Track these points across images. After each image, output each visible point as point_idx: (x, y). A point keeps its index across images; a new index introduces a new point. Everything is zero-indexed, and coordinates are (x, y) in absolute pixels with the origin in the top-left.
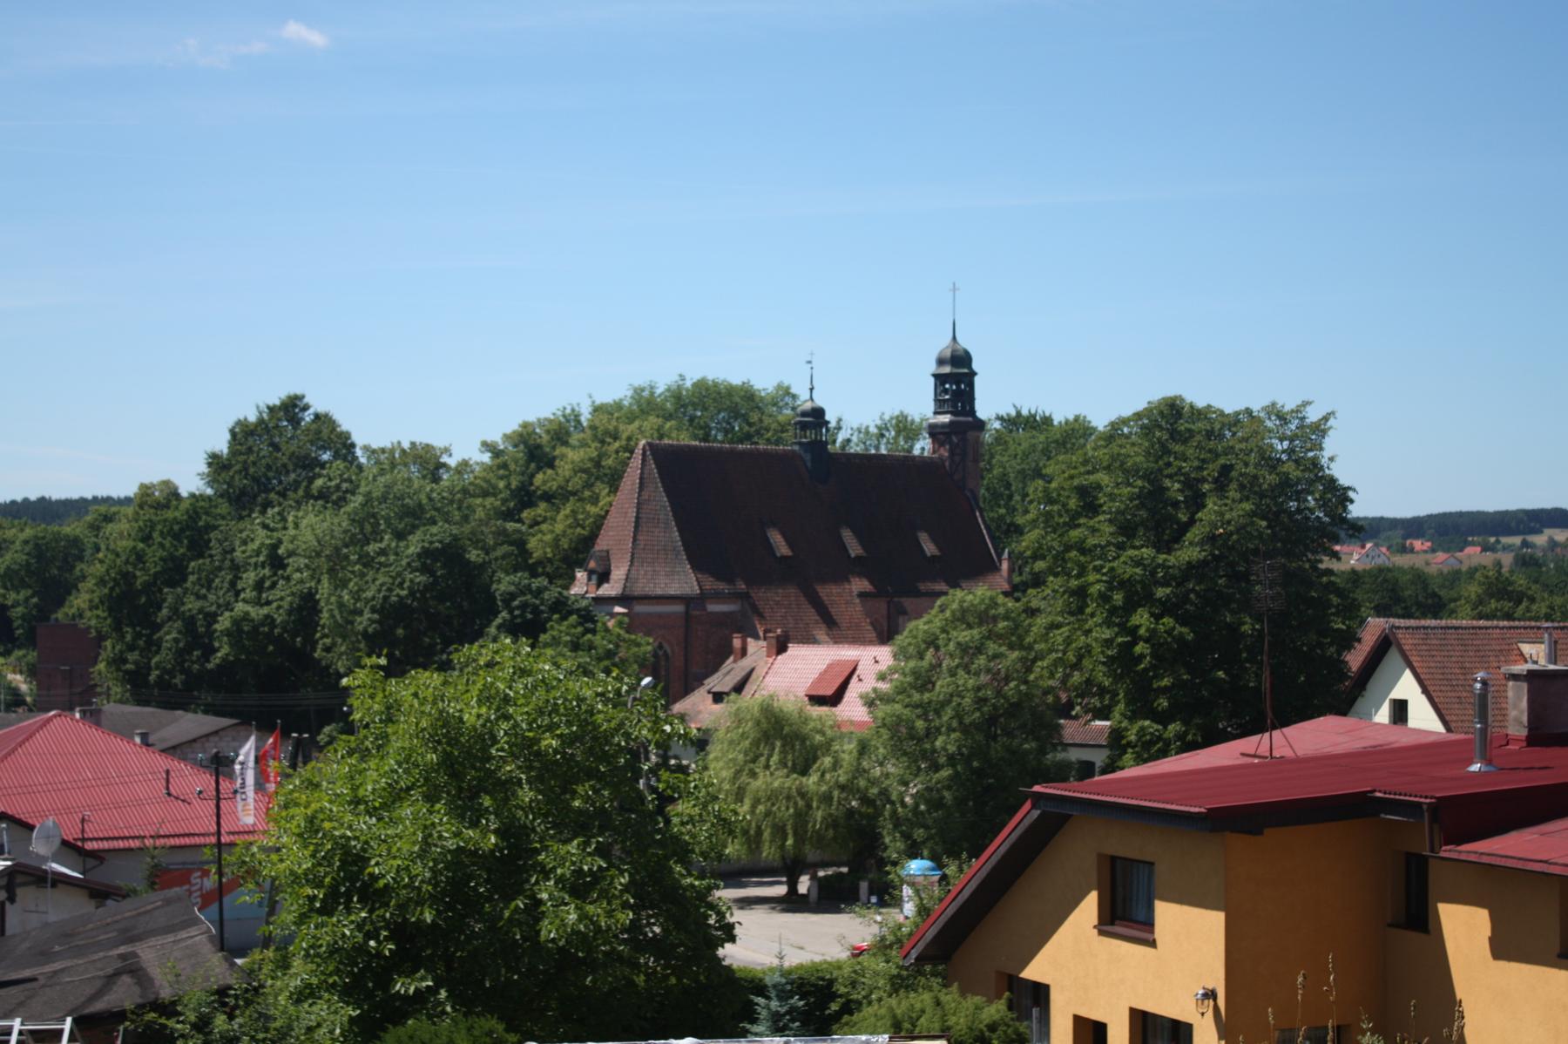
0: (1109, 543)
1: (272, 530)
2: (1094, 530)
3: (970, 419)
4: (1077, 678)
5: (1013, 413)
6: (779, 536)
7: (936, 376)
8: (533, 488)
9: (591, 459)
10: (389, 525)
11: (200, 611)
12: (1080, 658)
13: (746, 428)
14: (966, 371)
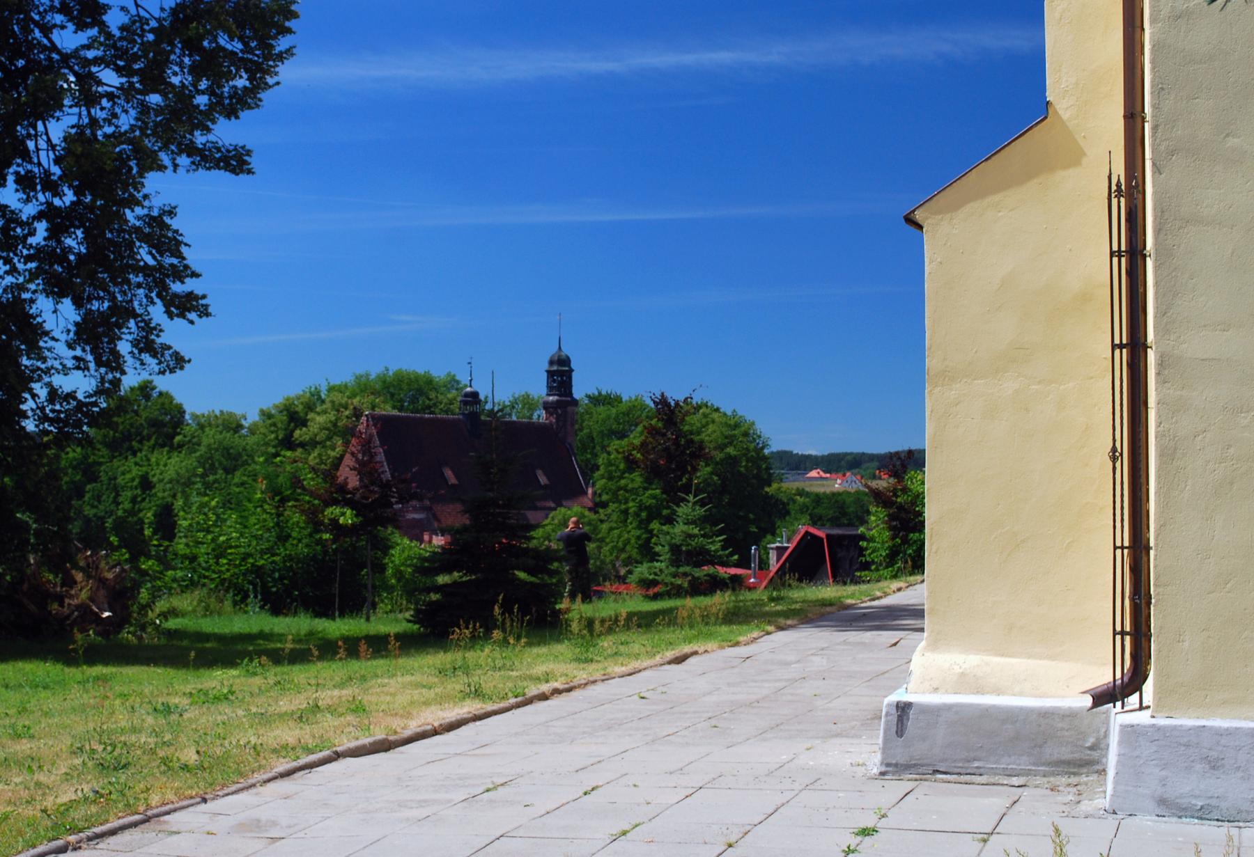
0: (640, 487)
1: (141, 466)
2: (633, 480)
3: (569, 399)
4: (623, 556)
5: (597, 393)
6: (450, 472)
7: (548, 372)
8: (293, 439)
9: (331, 421)
10: (221, 464)
11: (95, 515)
12: (625, 545)
13: (427, 402)
14: (567, 369)
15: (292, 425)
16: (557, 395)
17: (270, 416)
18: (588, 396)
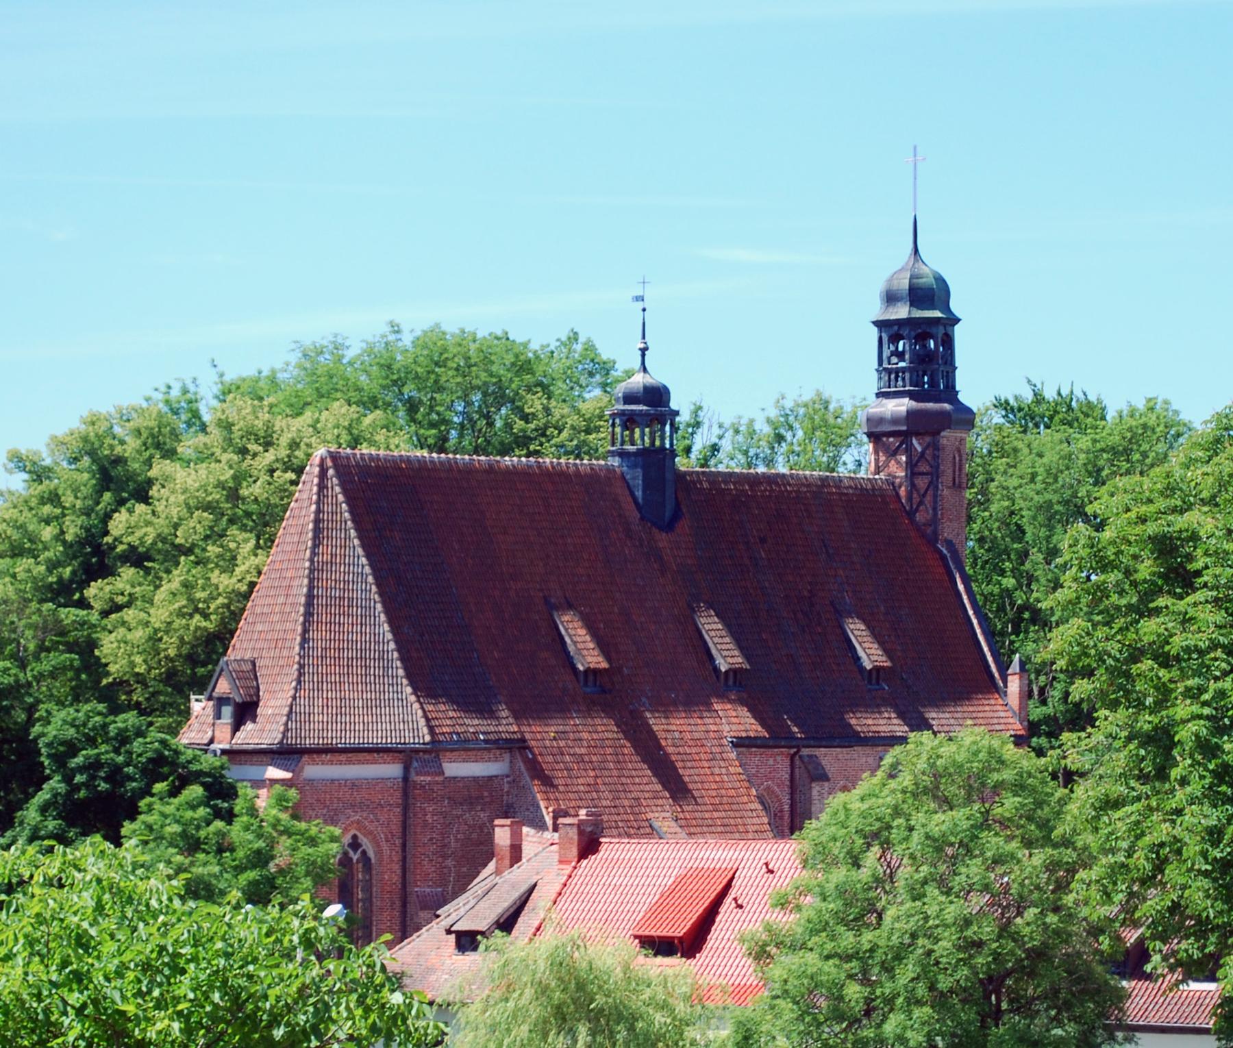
3: (947, 406)
5: (1028, 396)
7: (881, 324)
9: (221, 485)
13: (519, 424)
14: (937, 314)
15: (107, 496)
16: (912, 396)
17: (39, 474)
18: (1003, 405)
